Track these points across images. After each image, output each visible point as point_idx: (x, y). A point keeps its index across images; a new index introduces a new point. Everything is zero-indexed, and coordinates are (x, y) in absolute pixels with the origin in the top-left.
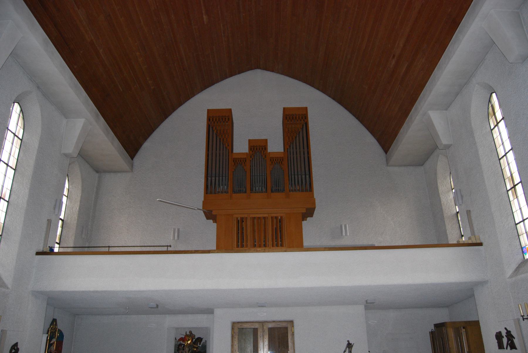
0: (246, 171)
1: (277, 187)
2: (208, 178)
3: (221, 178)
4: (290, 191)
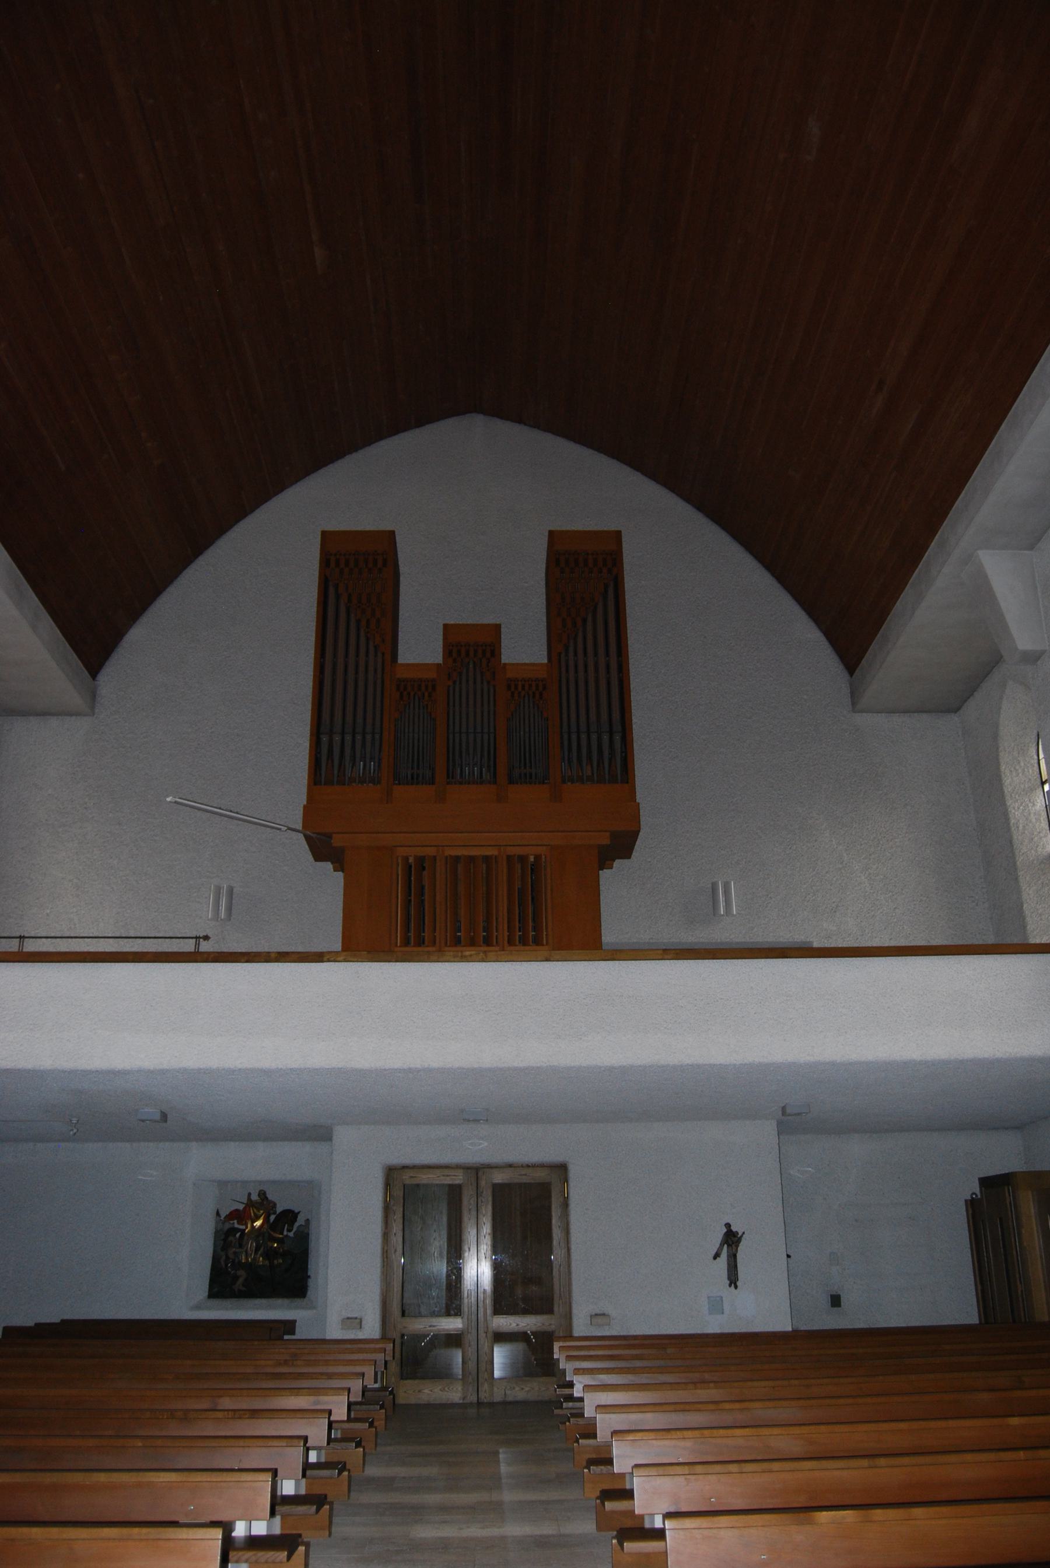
1: (525, 768)
2: (322, 736)
3: (359, 737)
4: (564, 782)
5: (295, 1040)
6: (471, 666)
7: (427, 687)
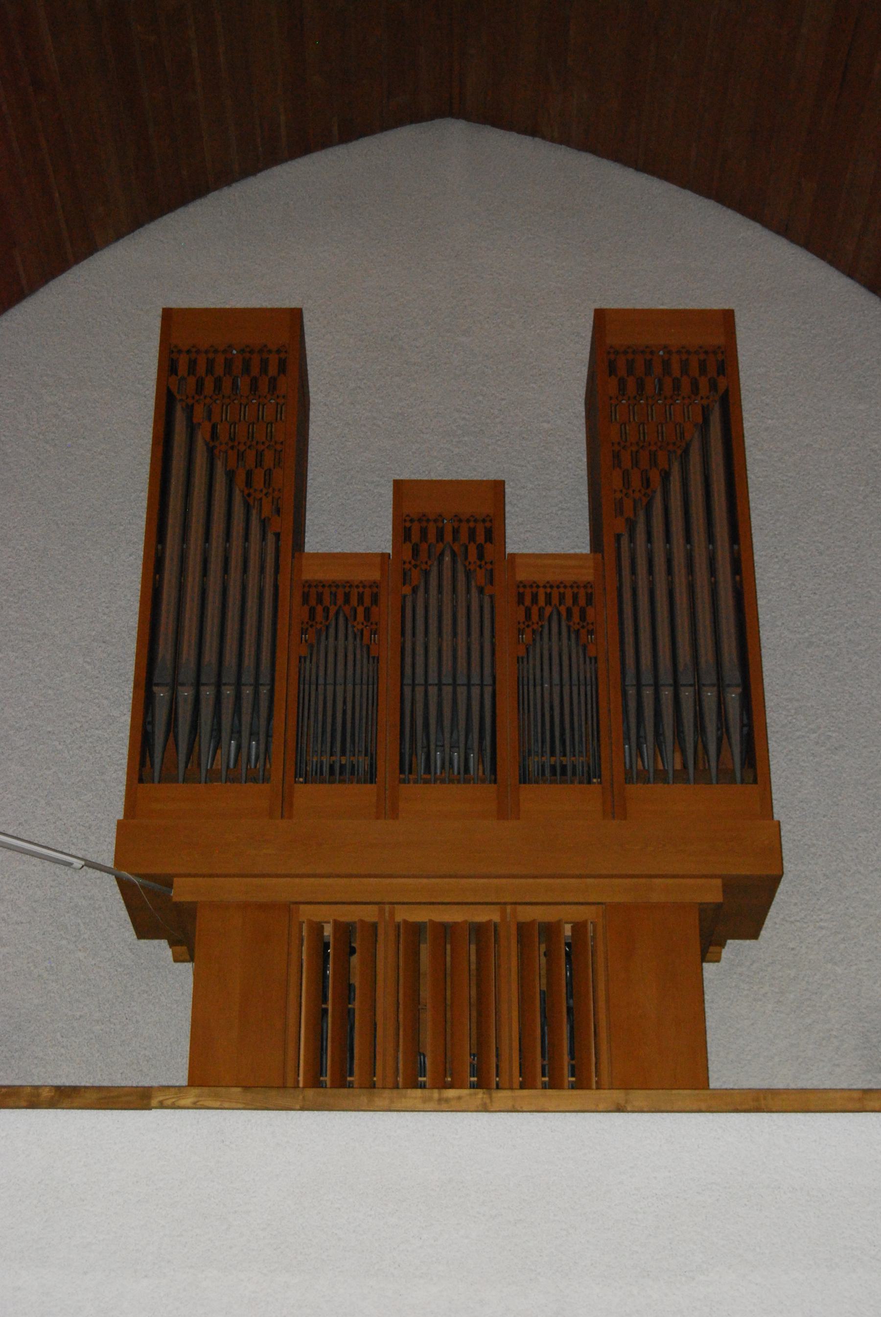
0: (377, 660)
1: (553, 753)
2: (155, 689)
3: (228, 692)
4: (629, 780)
5: (85, 1273)
6: (447, 559)
7: (361, 597)
